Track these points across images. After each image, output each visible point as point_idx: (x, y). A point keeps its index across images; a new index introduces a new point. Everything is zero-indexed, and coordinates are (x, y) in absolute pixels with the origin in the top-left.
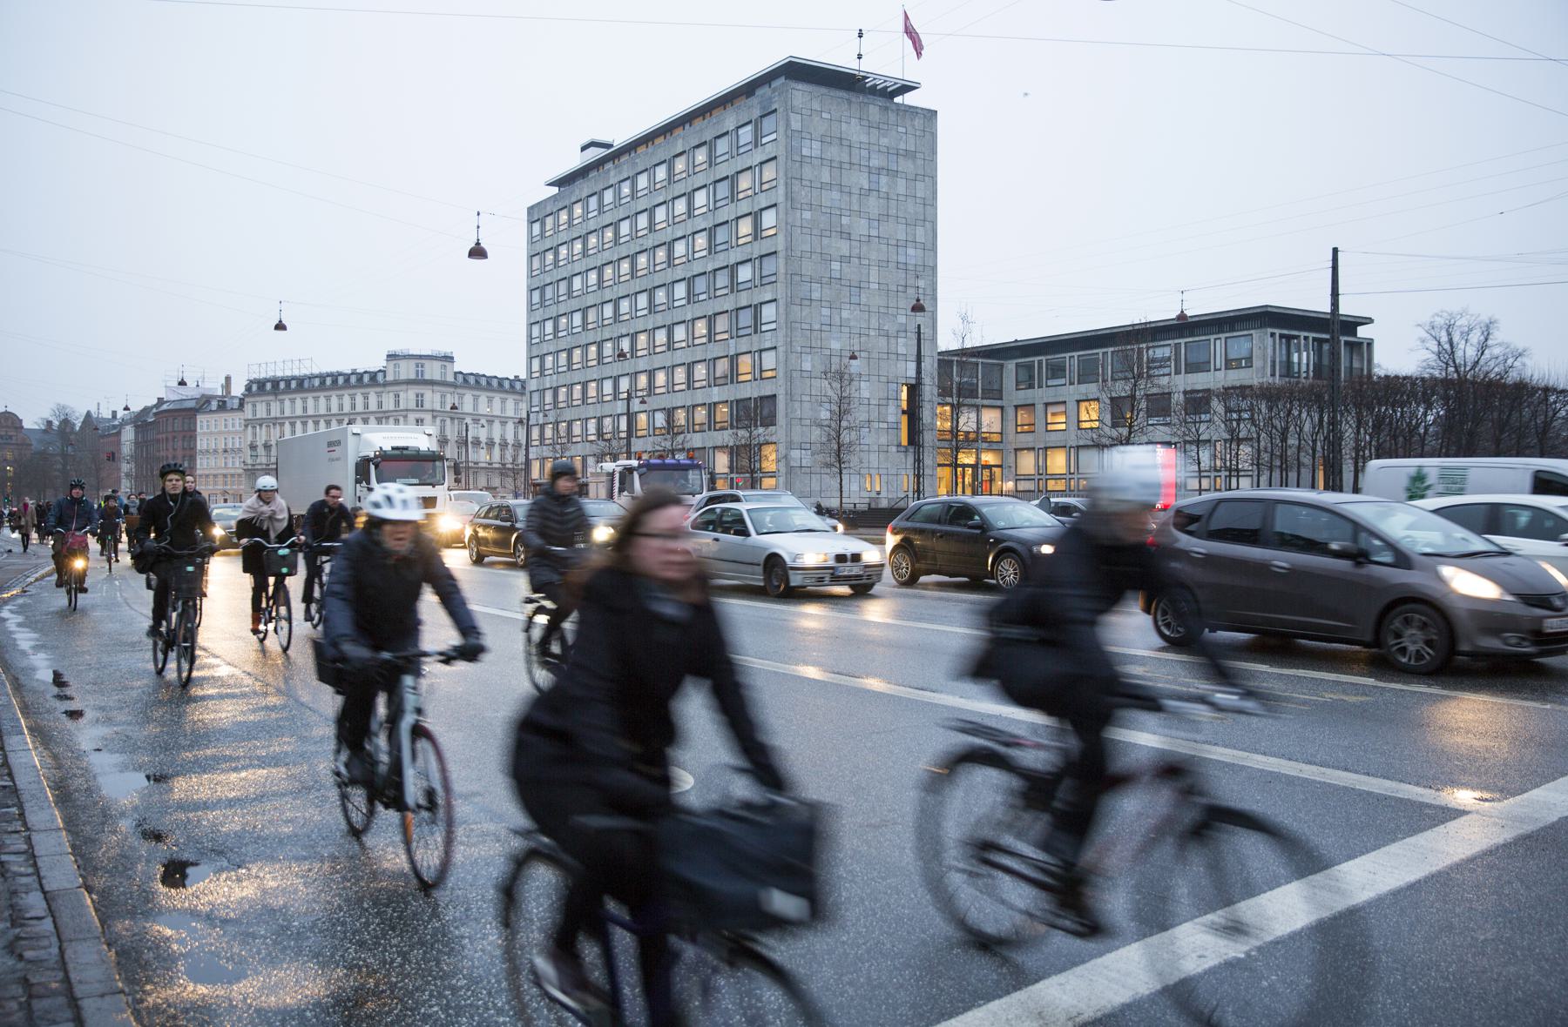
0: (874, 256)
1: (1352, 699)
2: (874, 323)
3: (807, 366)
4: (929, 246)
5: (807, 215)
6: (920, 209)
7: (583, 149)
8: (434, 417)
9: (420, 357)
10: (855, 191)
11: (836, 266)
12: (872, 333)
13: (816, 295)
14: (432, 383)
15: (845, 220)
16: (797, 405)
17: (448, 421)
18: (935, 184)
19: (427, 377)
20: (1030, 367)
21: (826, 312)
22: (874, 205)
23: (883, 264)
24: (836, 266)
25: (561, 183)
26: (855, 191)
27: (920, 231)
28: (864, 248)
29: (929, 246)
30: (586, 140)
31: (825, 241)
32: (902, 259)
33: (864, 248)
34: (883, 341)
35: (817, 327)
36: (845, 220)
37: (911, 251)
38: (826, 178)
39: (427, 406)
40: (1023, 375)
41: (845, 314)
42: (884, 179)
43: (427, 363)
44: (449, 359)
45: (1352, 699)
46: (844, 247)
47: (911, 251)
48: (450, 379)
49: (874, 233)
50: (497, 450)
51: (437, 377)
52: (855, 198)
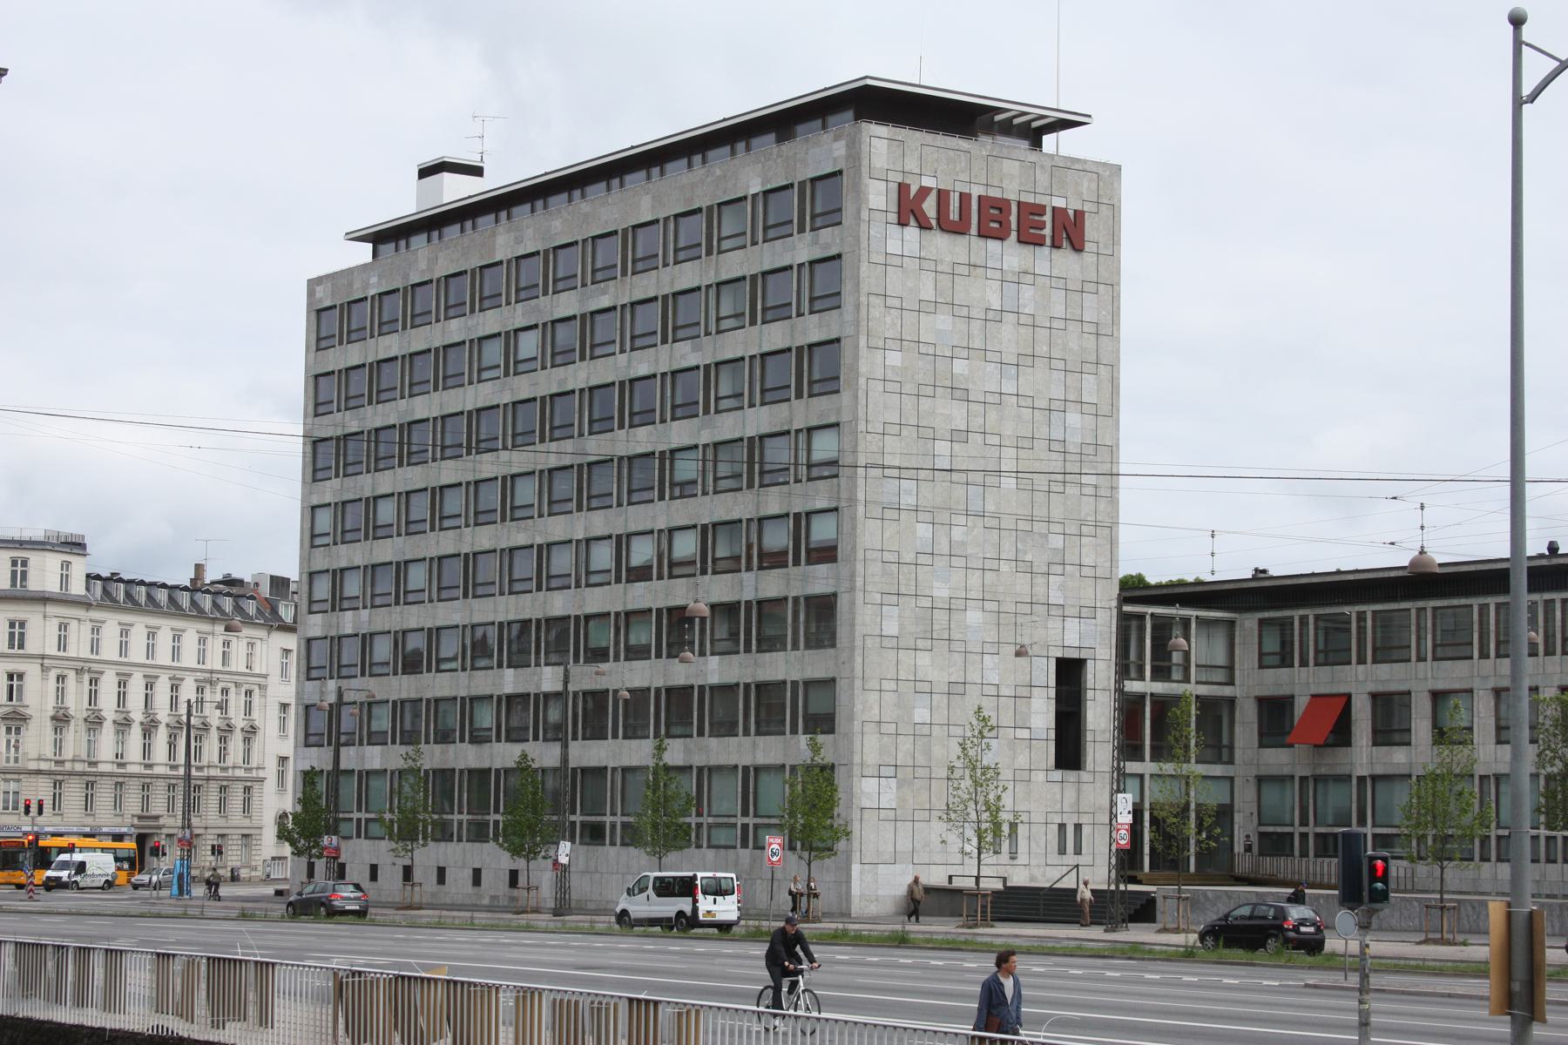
0: (1008, 430)
1: (802, 617)
2: (1008, 551)
3: (891, 628)
4: (1105, 409)
5: (894, 359)
6: (1090, 342)
7: (425, 172)
8: (44, 669)
9: (21, 544)
10: (977, 313)
11: (942, 447)
12: (1005, 567)
13: (908, 500)
14: (44, 599)
15: (960, 367)
16: (874, 696)
17: (72, 675)
18: (1115, 299)
19: (34, 585)
20: (1285, 626)
21: (923, 531)
22: (1008, 338)
23: (1024, 443)
24: (942, 447)
25: (381, 238)
26: (977, 313)
27: (1089, 382)
28: (992, 415)
29: (1105, 409)
30: (430, 158)
31: (925, 404)
32: (1057, 434)
33: (992, 415)
34: (1022, 582)
35: (908, 557)
36: (960, 367)
37: (1073, 418)
38: (928, 293)
39: (32, 646)
40: (1272, 644)
41: (957, 534)
42: (1027, 293)
43: (34, 558)
44: (76, 546)
45: (802, 617)
46: (957, 415)
47: (1073, 418)
48: (77, 588)
49: (1009, 387)
50: (135, 736)
51: (52, 586)
52: (976, 326)
